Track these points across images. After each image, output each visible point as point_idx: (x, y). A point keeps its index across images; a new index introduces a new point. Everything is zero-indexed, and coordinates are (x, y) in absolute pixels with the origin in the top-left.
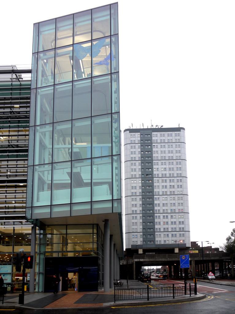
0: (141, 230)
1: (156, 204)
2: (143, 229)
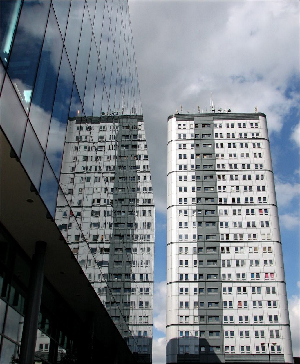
0: (197, 320)
1: (224, 261)
2: (201, 318)
